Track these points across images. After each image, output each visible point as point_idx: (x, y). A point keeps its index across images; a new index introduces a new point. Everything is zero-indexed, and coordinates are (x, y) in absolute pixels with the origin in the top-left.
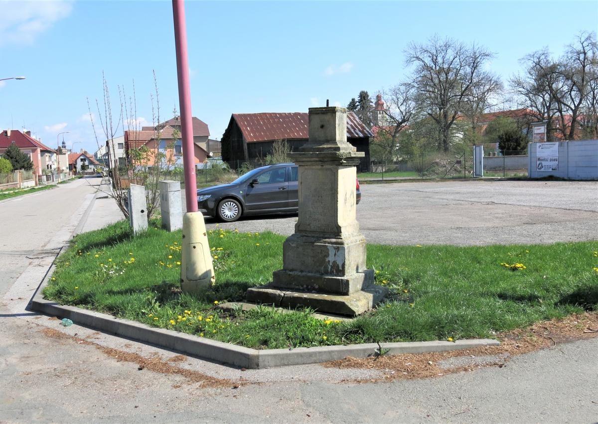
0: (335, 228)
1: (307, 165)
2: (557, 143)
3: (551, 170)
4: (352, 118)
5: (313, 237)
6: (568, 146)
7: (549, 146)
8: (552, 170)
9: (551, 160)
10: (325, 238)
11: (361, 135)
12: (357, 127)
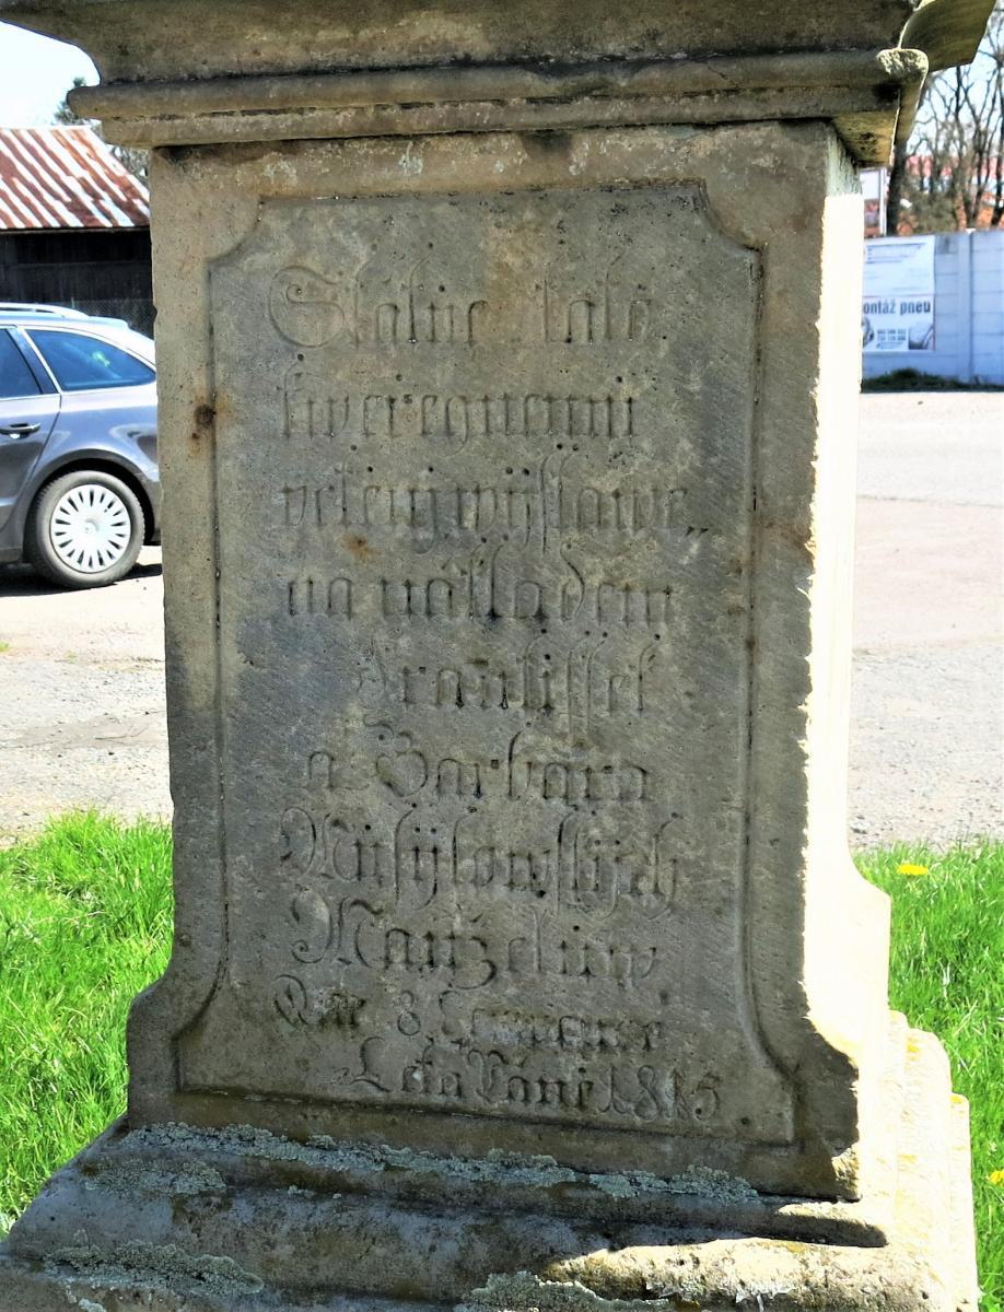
0: (762, 1073)
1: (289, 146)
2: (929, 242)
3: (904, 348)
4: (83, 151)
5: (413, 1198)
6: (971, 251)
7: (896, 252)
8: (912, 346)
9: (904, 309)
10: (618, 1228)
11: (125, 221)
12: (105, 187)
